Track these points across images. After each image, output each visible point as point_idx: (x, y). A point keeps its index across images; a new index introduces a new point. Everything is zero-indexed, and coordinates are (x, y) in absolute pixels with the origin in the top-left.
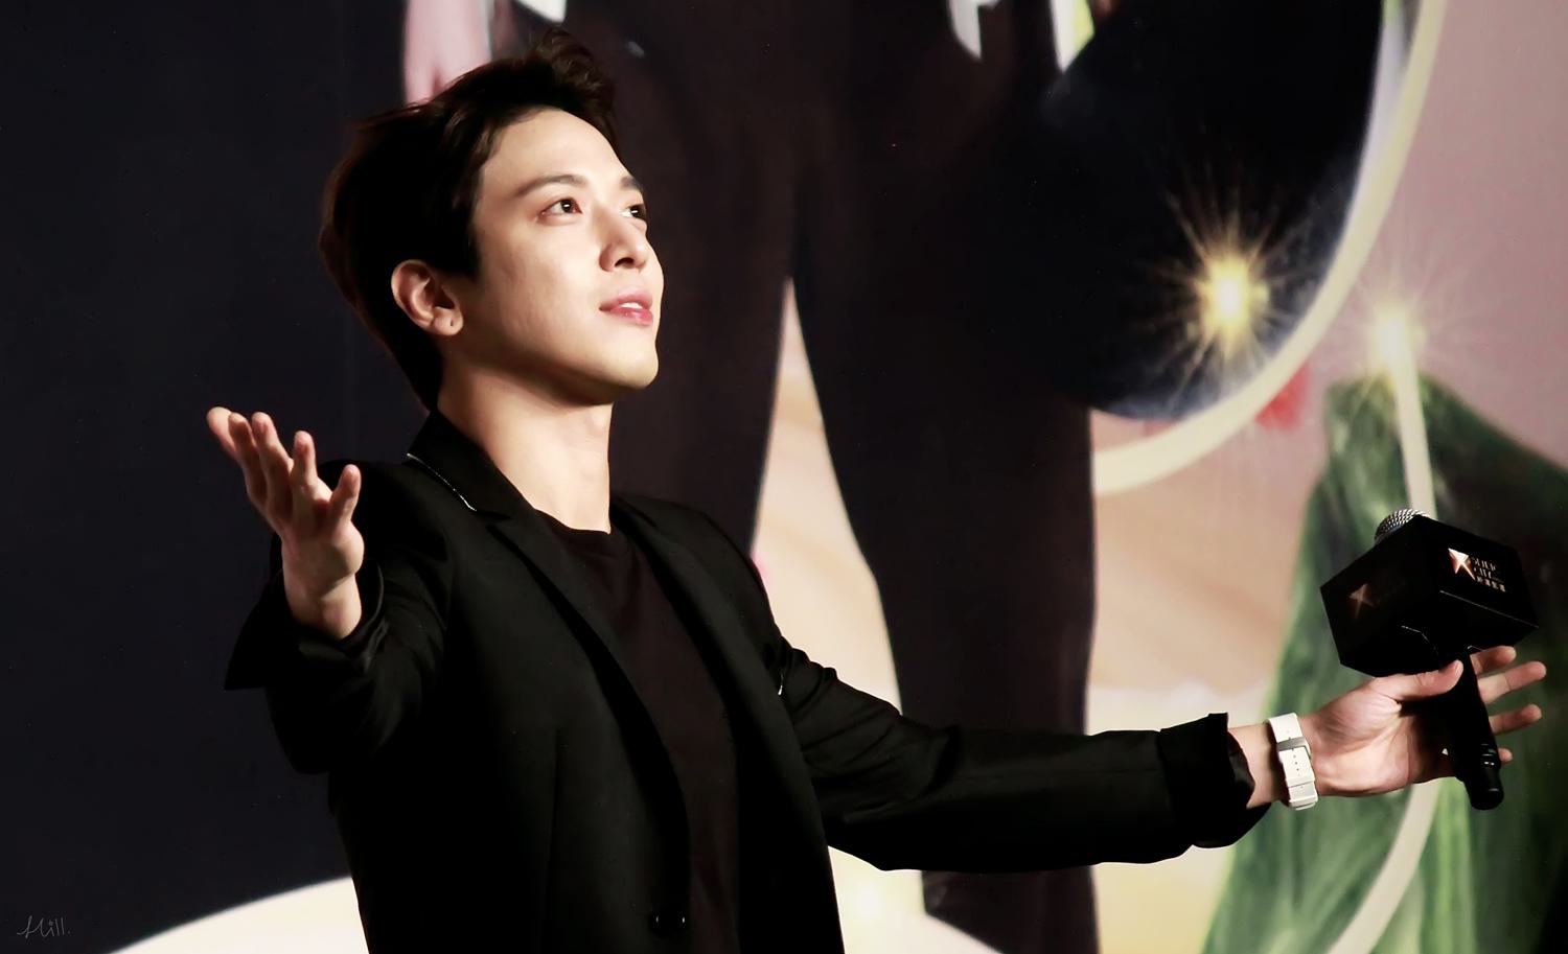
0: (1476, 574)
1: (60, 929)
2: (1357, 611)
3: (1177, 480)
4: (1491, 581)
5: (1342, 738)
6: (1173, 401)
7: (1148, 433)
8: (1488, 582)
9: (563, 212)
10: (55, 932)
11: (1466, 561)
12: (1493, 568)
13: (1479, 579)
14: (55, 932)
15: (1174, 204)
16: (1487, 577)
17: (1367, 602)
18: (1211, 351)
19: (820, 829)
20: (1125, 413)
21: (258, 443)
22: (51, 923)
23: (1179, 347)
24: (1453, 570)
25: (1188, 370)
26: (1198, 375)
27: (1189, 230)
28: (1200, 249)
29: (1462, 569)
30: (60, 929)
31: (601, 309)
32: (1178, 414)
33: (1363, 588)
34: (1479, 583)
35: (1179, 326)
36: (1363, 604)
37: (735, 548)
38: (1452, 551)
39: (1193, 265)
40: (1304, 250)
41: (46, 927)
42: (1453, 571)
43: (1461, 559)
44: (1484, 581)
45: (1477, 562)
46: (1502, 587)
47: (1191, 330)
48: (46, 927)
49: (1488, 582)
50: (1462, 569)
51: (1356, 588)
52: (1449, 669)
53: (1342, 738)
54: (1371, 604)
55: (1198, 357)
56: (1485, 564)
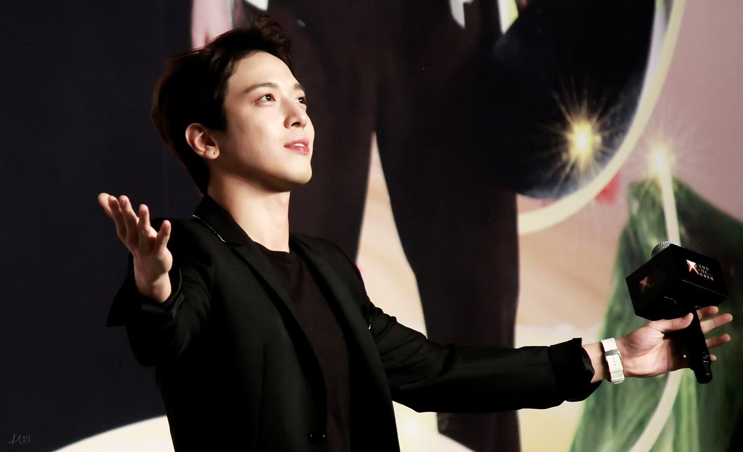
0: (699, 272)
1: (29, 440)
3: (558, 228)
4: (706, 275)
5: (636, 350)
6: (556, 190)
7: (544, 205)
8: (705, 276)
9: (267, 100)
10: (26, 442)
14: (26, 442)
15: (556, 96)
17: (648, 285)
18: (574, 166)
19: (389, 393)
20: (533, 196)
22: (24, 437)
23: (559, 165)
25: (563, 175)
26: (568, 178)
27: (563, 109)
28: (569, 118)
29: (693, 269)
30: (29, 440)
32: (558, 196)
33: (646, 279)
34: (701, 276)
35: (559, 154)
37: (348, 259)
38: (688, 261)
39: (565, 125)
40: (618, 119)
41: (22, 439)
42: (689, 270)
44: (703, 276)
47: (564, 156)
48: (22, 439)
50: (693, 269)
51: (643, 279)
52: (686, 317)
53: (636, 350)
54: (650, 286)
55: (568, 169)
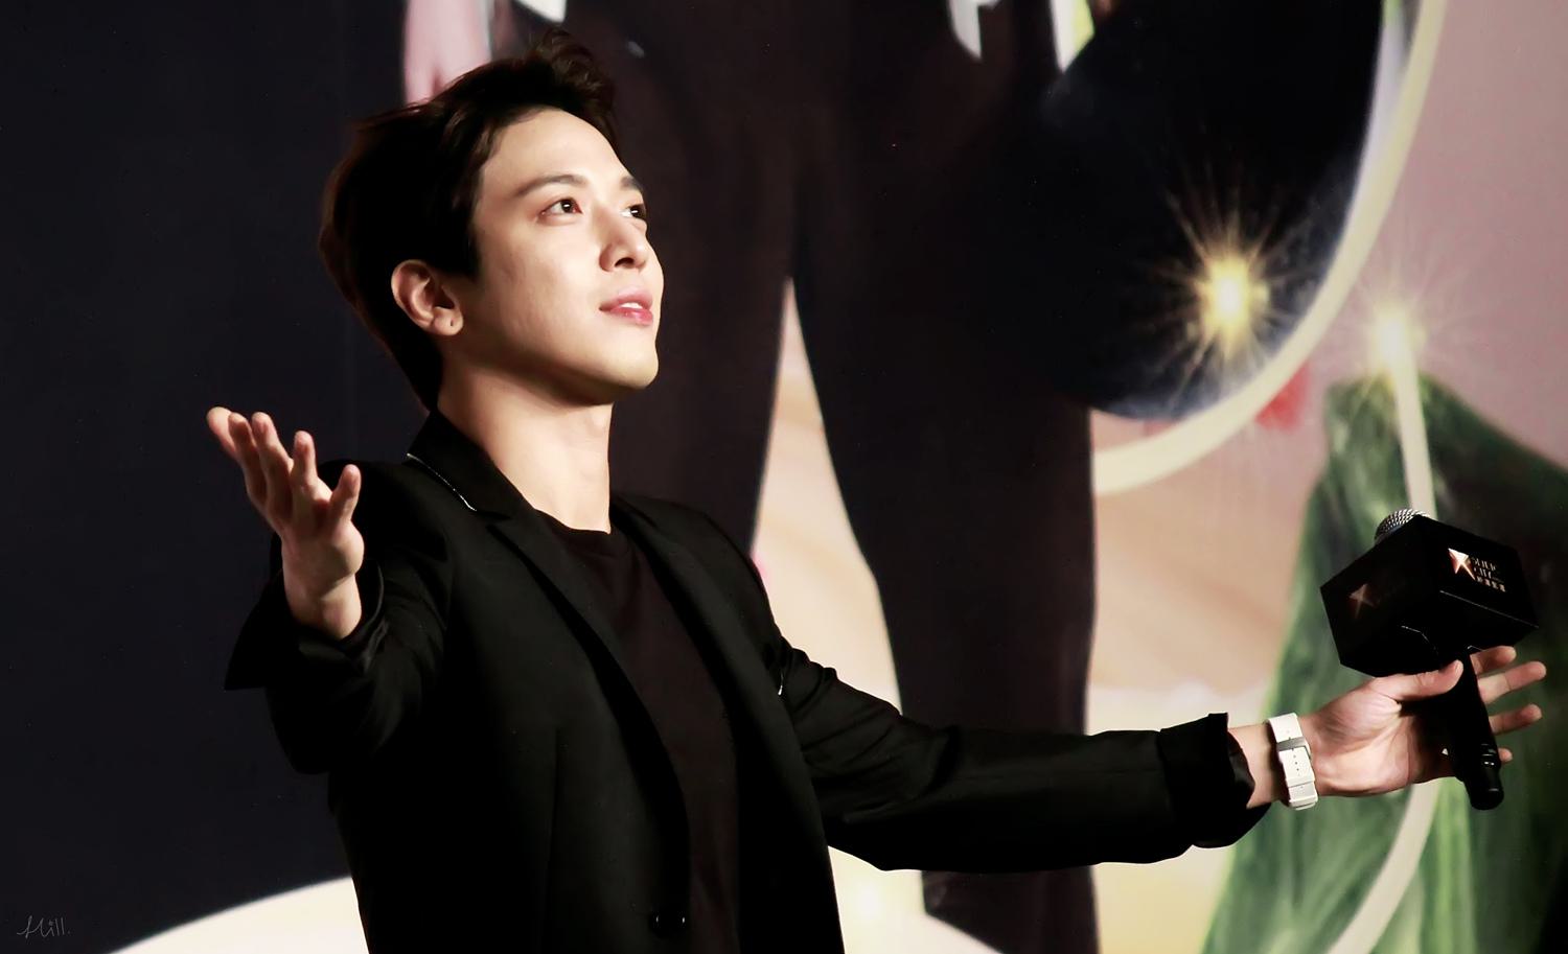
0: (1476, 574)
1: (60, 929)
2: (1357, 611)
3: (1177, 480)
4: (1491, 581)
5: (1342, 738)
6: (1173, 401)
7: (1148, 433)
8: (1488, 582)
9: (563, 212)
10: (55, 932)
11: (1466, 561)
12: (1493, 568)
13: (1479, 579)
14: (55, 932)
15: (1174, 204)
16: (1487, 577)
17: (1367, 602)
18: (1211, 351)
20: (1125, 413)
21: (258, 443)
22: (51, 923)
23: (1179, 347)
24: (1453, 570)
25: (1188, 370)
26: (1198, 375)
27: (1189, 230)
28: (1200, 249)
29: (1462, 569)
30: (60, 929)
31: (601, 309)
32: (1178, 414)
33: (1363, 588)
34: (1479, 583)
35: (1179, 326)
36: (1363, 604)
37: (735, 548)
38: (1452, 551)
39: (1193, 265)
40: (1304, 250)
41: (46, 927)
42: (1453, 571)
43: (1461, 559)
44: (1484, 581)
45: (1477, 562)
46: (1502, 587)
47: (1191, 330)
48: (46, 927)
49: (1488, 582)
50: (1462, 569)
51: (1356, 588)
52: (1449, 669)
53: (1342, 738)
54: (1371, 604)
55: (1198, 357)
56: (1485, 564)
